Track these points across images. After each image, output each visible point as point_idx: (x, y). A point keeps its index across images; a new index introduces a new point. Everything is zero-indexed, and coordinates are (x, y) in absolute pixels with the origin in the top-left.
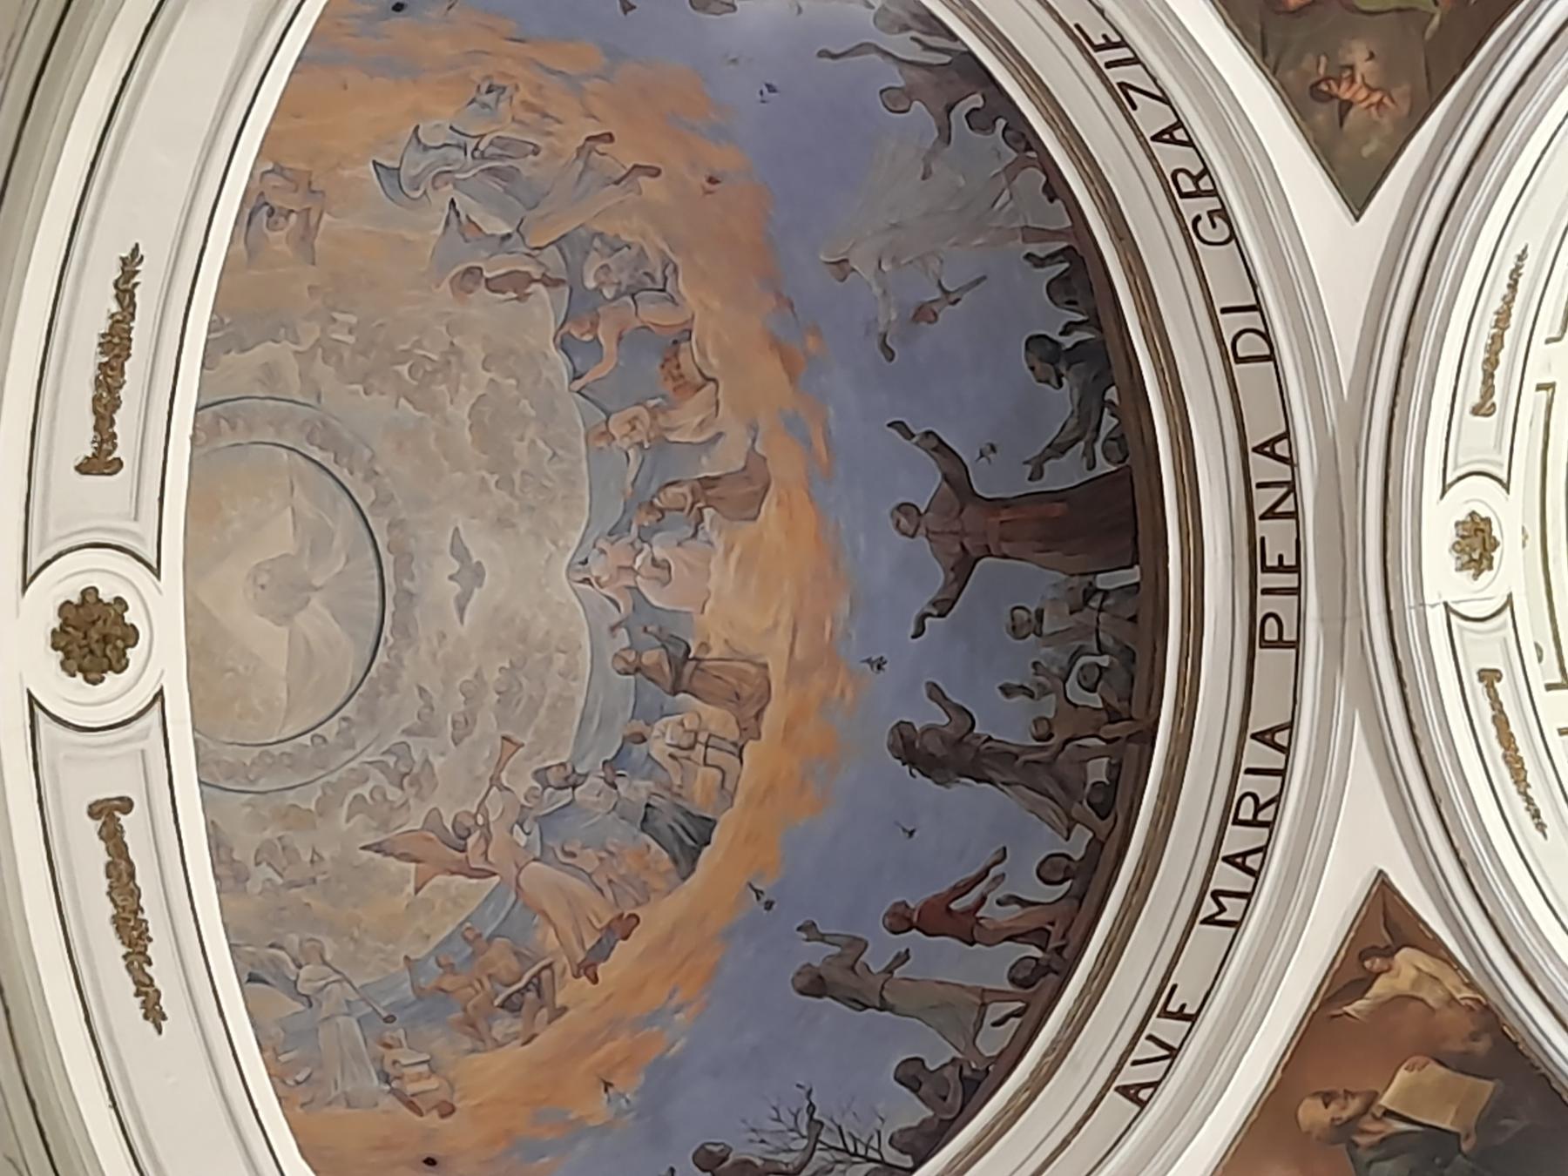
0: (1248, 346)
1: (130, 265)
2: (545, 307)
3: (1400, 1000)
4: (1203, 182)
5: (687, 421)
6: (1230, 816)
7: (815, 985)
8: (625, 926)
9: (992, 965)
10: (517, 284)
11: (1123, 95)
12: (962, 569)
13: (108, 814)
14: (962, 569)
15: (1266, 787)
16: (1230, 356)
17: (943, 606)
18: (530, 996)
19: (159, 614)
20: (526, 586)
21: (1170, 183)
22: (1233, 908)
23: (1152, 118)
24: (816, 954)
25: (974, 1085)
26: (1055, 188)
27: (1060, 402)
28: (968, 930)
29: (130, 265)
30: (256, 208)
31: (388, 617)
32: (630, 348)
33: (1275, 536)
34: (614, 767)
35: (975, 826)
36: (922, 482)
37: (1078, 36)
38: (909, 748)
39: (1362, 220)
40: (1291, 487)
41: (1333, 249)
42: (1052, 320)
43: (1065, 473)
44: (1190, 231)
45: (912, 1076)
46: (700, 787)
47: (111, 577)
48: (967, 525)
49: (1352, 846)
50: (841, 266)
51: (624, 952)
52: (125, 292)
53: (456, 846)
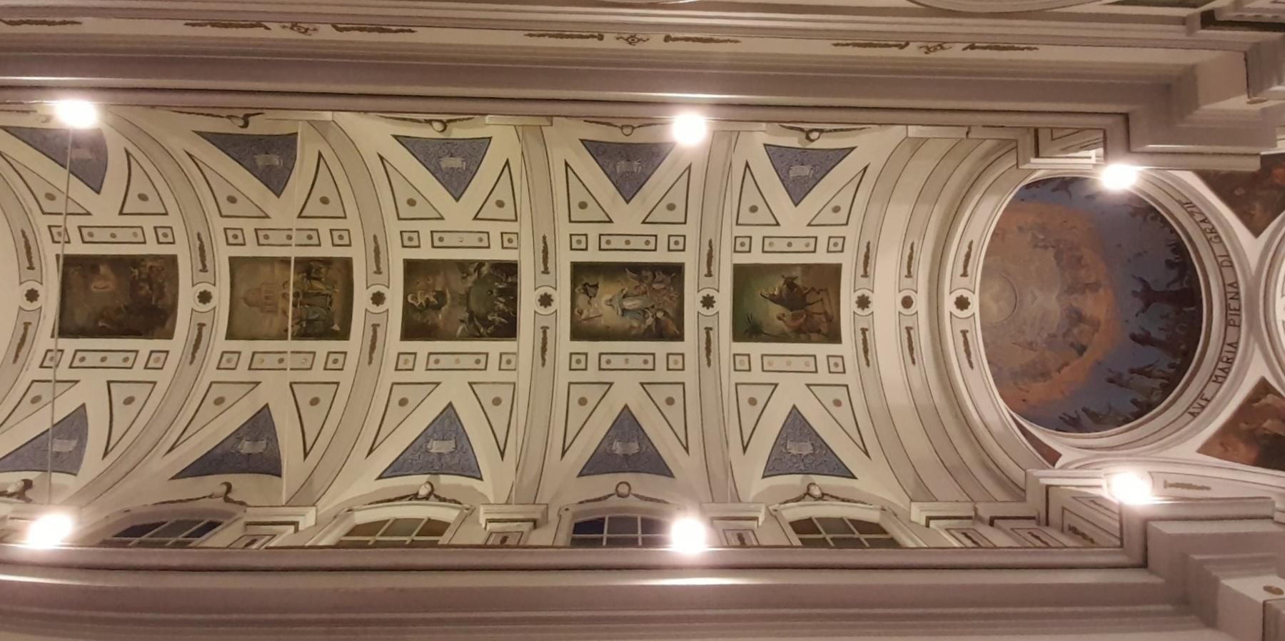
0: (1225, 263)
1: (971, 243)
2: (1051, 252)
3: (1268, 405)
4: (1213, 230)
5: (1083, 272)
6: (1220, 359)
7: (1111, 381)
8: (1066, 364)
9: (1156, 383)
10: (1046, 247)
11: (1192, 214)
12: (1147, 305)
13: (964, 333)
14: (1147, 305)
15: (1230, 355)
16: (1220, 266)
17: (1143, 311)
18: (1045, 375)
19: (974, 301)
20: (1046, 303)
21: (1204, 231)
22: (1220, 379)
23: (1198, 218)
24: (1111, 375)
25: (1151, 407)
26: (1173, 231)
27: (1174, 273)
28: (1149, 375)
29: (971, 243)
30: (994, 234)
31: (1016, 304)
32: (1068, 258)
33: (1233, 304)
34: (1065, 335)
35: (1149, 356)
36: (1139, 289)
37: (1179, 202)
38: (1134, 338)
39: (103, 190)
40: (1238, 293)
41: (1250, 246)
42: (1172, 257)
43: (1176, 287)
44: (1209, 241)
45: (1135, 402)
46: (1084, 341)
47: (966, 294)
48: (1149, 296)
49: (1255, 370)
50: (1119, 246)
51: (1066, 370)
52: (970, 247)
53: (1030, 345)
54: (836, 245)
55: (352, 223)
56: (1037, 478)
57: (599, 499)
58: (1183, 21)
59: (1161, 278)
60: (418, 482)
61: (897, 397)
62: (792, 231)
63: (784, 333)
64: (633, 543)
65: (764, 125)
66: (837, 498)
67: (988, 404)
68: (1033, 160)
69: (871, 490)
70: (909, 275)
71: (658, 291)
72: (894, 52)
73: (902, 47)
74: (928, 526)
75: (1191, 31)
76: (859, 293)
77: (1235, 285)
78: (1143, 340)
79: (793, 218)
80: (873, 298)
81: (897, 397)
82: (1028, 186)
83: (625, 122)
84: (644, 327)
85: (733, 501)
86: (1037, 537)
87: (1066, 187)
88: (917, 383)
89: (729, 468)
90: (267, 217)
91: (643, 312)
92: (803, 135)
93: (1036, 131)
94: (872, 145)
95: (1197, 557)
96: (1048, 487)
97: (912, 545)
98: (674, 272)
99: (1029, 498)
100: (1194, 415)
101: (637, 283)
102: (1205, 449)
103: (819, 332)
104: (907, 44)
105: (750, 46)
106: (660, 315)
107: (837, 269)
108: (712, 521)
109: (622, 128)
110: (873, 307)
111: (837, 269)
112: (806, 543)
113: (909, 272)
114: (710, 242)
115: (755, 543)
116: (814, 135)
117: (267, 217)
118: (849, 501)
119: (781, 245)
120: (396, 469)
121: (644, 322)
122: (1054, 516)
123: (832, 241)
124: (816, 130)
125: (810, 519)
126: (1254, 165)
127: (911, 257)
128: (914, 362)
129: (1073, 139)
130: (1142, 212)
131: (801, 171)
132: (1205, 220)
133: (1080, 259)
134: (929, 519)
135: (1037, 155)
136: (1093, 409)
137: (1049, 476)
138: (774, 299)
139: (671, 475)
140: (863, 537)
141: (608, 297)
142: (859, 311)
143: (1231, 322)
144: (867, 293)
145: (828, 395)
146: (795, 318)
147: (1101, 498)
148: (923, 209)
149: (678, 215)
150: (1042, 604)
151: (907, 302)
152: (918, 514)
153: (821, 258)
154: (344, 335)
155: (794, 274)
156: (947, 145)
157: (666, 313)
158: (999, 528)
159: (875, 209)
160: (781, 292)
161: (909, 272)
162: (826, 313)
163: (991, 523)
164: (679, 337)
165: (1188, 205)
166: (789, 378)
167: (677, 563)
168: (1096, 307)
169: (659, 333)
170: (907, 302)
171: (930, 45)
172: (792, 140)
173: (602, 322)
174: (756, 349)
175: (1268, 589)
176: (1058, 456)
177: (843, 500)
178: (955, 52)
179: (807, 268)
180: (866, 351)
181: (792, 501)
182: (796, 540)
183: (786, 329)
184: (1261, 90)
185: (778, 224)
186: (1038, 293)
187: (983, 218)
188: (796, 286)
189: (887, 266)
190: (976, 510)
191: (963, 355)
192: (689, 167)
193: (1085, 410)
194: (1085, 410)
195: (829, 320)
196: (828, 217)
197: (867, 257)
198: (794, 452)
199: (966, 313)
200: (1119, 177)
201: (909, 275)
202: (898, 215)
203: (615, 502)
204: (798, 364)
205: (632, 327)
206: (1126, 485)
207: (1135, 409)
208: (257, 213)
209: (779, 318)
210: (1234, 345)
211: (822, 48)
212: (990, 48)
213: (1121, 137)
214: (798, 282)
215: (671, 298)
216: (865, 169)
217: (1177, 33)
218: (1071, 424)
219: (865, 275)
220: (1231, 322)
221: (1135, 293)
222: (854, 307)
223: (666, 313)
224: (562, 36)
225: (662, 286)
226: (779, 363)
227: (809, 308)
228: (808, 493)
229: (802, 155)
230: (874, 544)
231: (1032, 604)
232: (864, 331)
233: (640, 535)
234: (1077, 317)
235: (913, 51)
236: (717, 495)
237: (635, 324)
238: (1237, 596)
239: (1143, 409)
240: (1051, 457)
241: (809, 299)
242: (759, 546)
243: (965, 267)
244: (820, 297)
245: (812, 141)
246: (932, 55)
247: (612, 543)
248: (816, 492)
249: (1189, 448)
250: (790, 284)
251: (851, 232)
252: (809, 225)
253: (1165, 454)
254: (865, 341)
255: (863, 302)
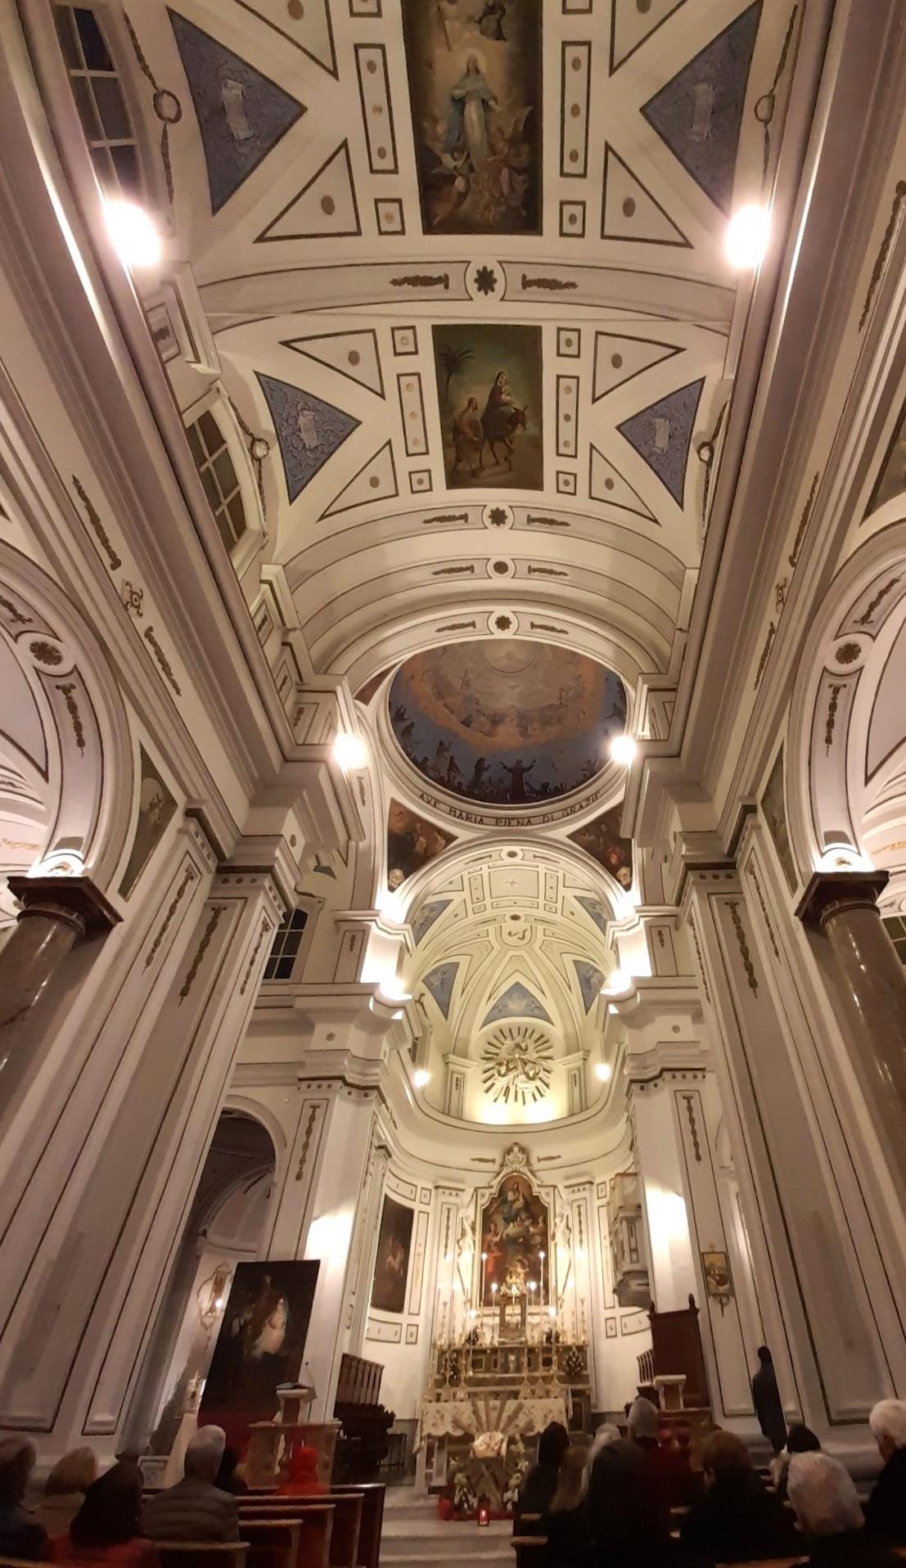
0: (546, 818)
2: (556, 702)
9: (444, 773)
12: (510, 770)
13: (473, 624)
16: (545, 815)
18: (439, 695)
20: (508, 697)
27: (538, 788)
30: (574, 654)
31: (505, 673)
33: (514, 822)
36: (525, 765)
43: (526, 788)
45: (426, 759)
47: (513, 626)
48: (518, 771)
53: (466, 683)
54: (567, 483)
55: (580, 502)
56: (340, 684)
57: (141, 58)
58: (752, 794)
59: (534, 778)
60: (265, 424)
61: (396, 554)
62: (585, 420)
63: (452, 410)
64: (91, 132)
65: (733, 377)
66: (260, 479)
67: (405, 643)
68: (646, 687)
69: (284, 523)
70: (531, 570)
71: (497, 181)
72: (788, 549)
73: (791, 559)
74: (262, 582)
75: (741, 798)
76: (508, 513)
77: (529, 823)
78: (480, 766)
79: (600, 424)
80: (503, 530)
81: (396, 554)
82: (621, 685)
83: (779, 105)
84: (437, 148)
85: (210, 323)
86: (284, 682)
87: (618, 714)
88: (415, 576)
89: (260, 315)
90: (612, 70)
91: (460, 147)
92: (707, 439)
93: (674, 690)
94: (682, 529)
95: (305, 793)
96: (334, 692)
97: (236, 564)
98: (524, 216)
99: (320, 677)
100: (422, 797)
101: (508, 132)
102: (394, 802)
103: (458, 460)
104: (793, 564)
105: (850, 343)
106: (460, 183)
107: (537, 484)
108: (167, 283)
109: (771, 96)
110: (493, 529)
111: (537, 484)
112: (190, 432)
113: (535, 570)
114: (573, 285)
115: (164, 356)
116: (705, 454)
117: (612, 70)
118: (261, 493)
119: (567, 407)
120: (269, 385)
121: (445, 151)
122: (308, 697)
123: (571, 478)
124: (711, 457)
125: (224, 442)
126: (625, 833)
127: (551, 572)
128: (436, 573)
129: (662, 715)
130: (591, 768)
131: (661, 435)
132: (582, 807)
133: (549, 723)
134: (270, 584)
135: (650, 690)
136: (414, 731)
137: (344, 695)
138: (495, 393)
139: (215, 209)
140: (223, 507)
141: (483, 66)
142: (487, 512)
143: (498, 820)
144: (509, 522)
145: (380, 468)
146: (472, 424)
147: (336, 732)
148: (604, 585)
149: (600, 491)
150: (96, 389)
151: (501, 567)
152: (270, 571)
153: (551, 464)
154: (430, 227)
155: (529, 424)
156: (670, 607)
157: (463, 196)
158: (282, 652)
159: (609, 533)
160: (506, 404)
161: (535, 570)
162: (482, 468)
163: (284, 644)
164: (429, 228)
165: (594, 797)
166: (394, 416)
167: (86, 208)
168: (507, 736)
169: (431, 184)
170: (501, 567)
171: (786, 590)
172: (703, 423)
173: (439, 53)
174: (426, 362)
175: (293, 838)
176: (366, 702)
177: (260, 486)
178: (771, 615)
179: (537, 444)
180: (442, 519)
181: (238, 417)
182: (190, 418)
183: (457, 413)
184: (684, 840)
185: (594, 400)
186: (517, 690)
187: (591, 644)
188: (514, 428)
189: (542, 546)
190: (294, 629)
191: (449, 623)
192: (687, 244)
193: (412, 725)
194: (412, 725)
195: (474, 474)
196: (602, 472)
197: (551, 522)
198: (301, 420)
199: (493, 627)
200: (624, 750)
201: (531, 570)
202: (599, 558)
203: (145, 93)
204: (414, 428)
205: (435, 121)
206: (353, 749)
207: (420, 760)
208: (619, 55)
209: (470, 401)
210: (481, 822)
211: (816, 461)
212: (766, 649)
213: (659, 751)
214: (519, 431)
215: (487, 207)
216: (656, 521)
217: (743, 789)
218: (398, 715)
219: (530, 520)
220: (498, 820)
221: (519, 762)
222: (492, 506)
223: (463, 196)
224: (804, 522)
225: (505, 189)
226: (411, 399)
227: (487, 444)
228: (254, 441)
229: (682, 437)
230: (221, 520)
231: (210, 657)
232: (465, 517)
233: (106, 143)
234: (496, 720)
235: (784, 570)
236: (214, 289)
237: (440, 129)
238: (283, 819)
239: (422, 765)
240: (364, 696)
241: (499, 446)
242: (163, 364)
243: (542, 627)
244: (501, 460)
245: (699, 452)
246: (774, 592)
247: (78, 84)
248: (260, 451)
249: (392, 792)
250: (517, 419)
251: (580, 502)
252: (592, 447)
253: (386, 780)
254: (461, 570)
255: (498, 517)
